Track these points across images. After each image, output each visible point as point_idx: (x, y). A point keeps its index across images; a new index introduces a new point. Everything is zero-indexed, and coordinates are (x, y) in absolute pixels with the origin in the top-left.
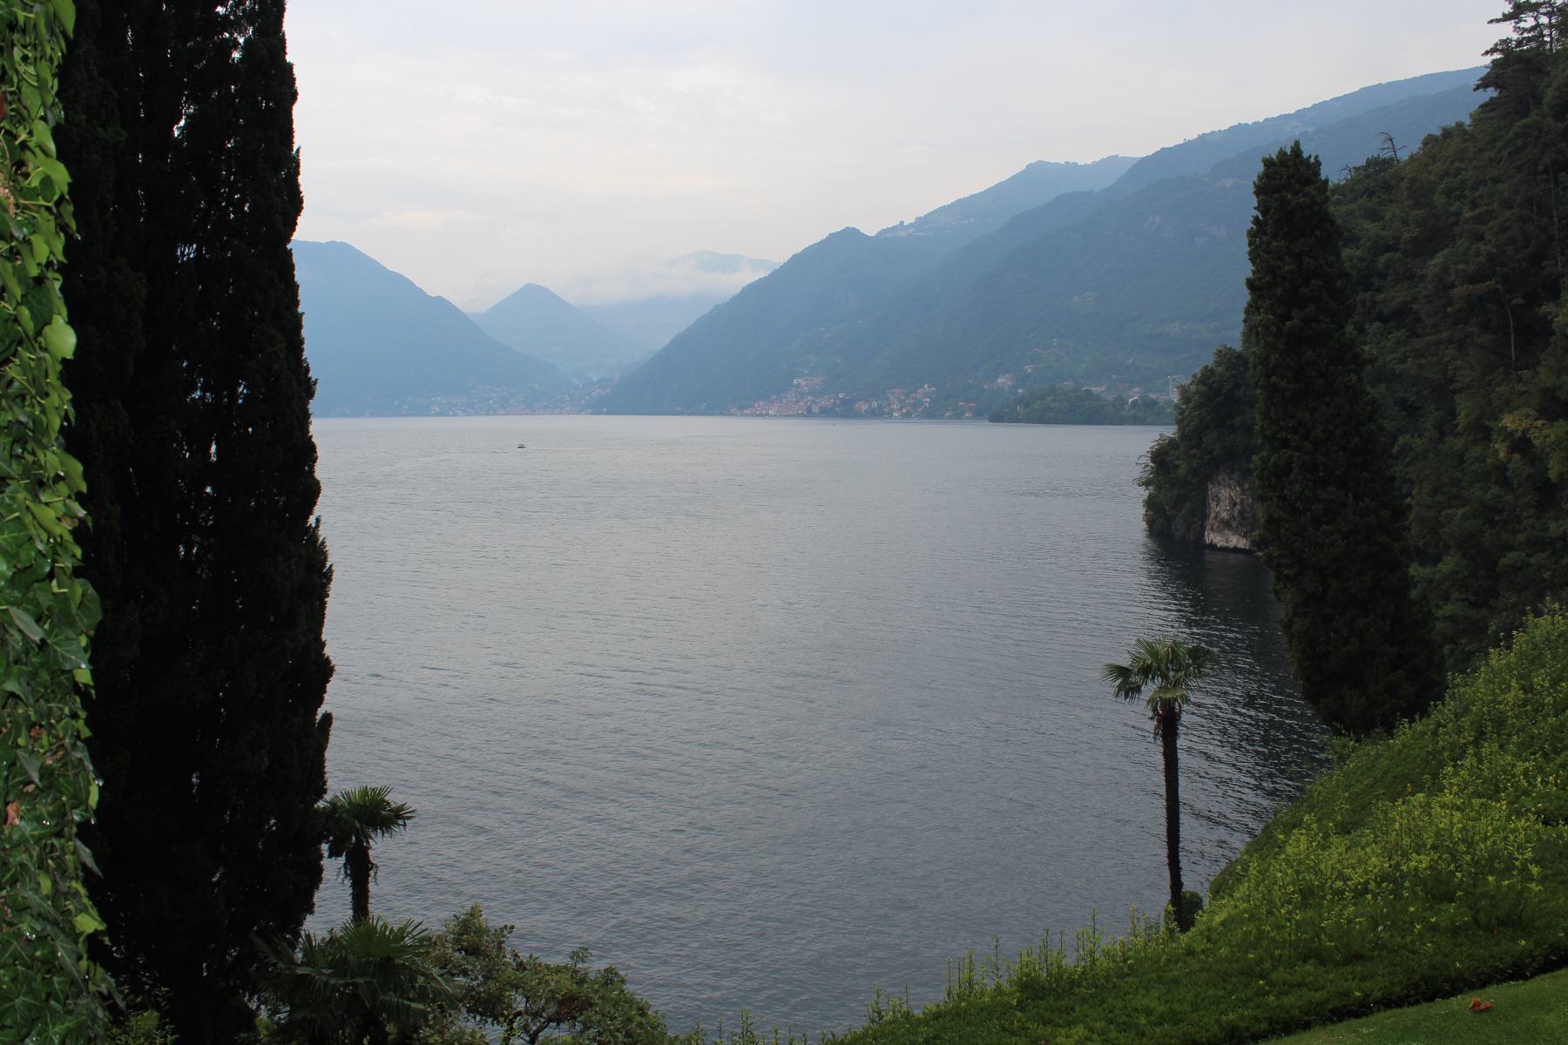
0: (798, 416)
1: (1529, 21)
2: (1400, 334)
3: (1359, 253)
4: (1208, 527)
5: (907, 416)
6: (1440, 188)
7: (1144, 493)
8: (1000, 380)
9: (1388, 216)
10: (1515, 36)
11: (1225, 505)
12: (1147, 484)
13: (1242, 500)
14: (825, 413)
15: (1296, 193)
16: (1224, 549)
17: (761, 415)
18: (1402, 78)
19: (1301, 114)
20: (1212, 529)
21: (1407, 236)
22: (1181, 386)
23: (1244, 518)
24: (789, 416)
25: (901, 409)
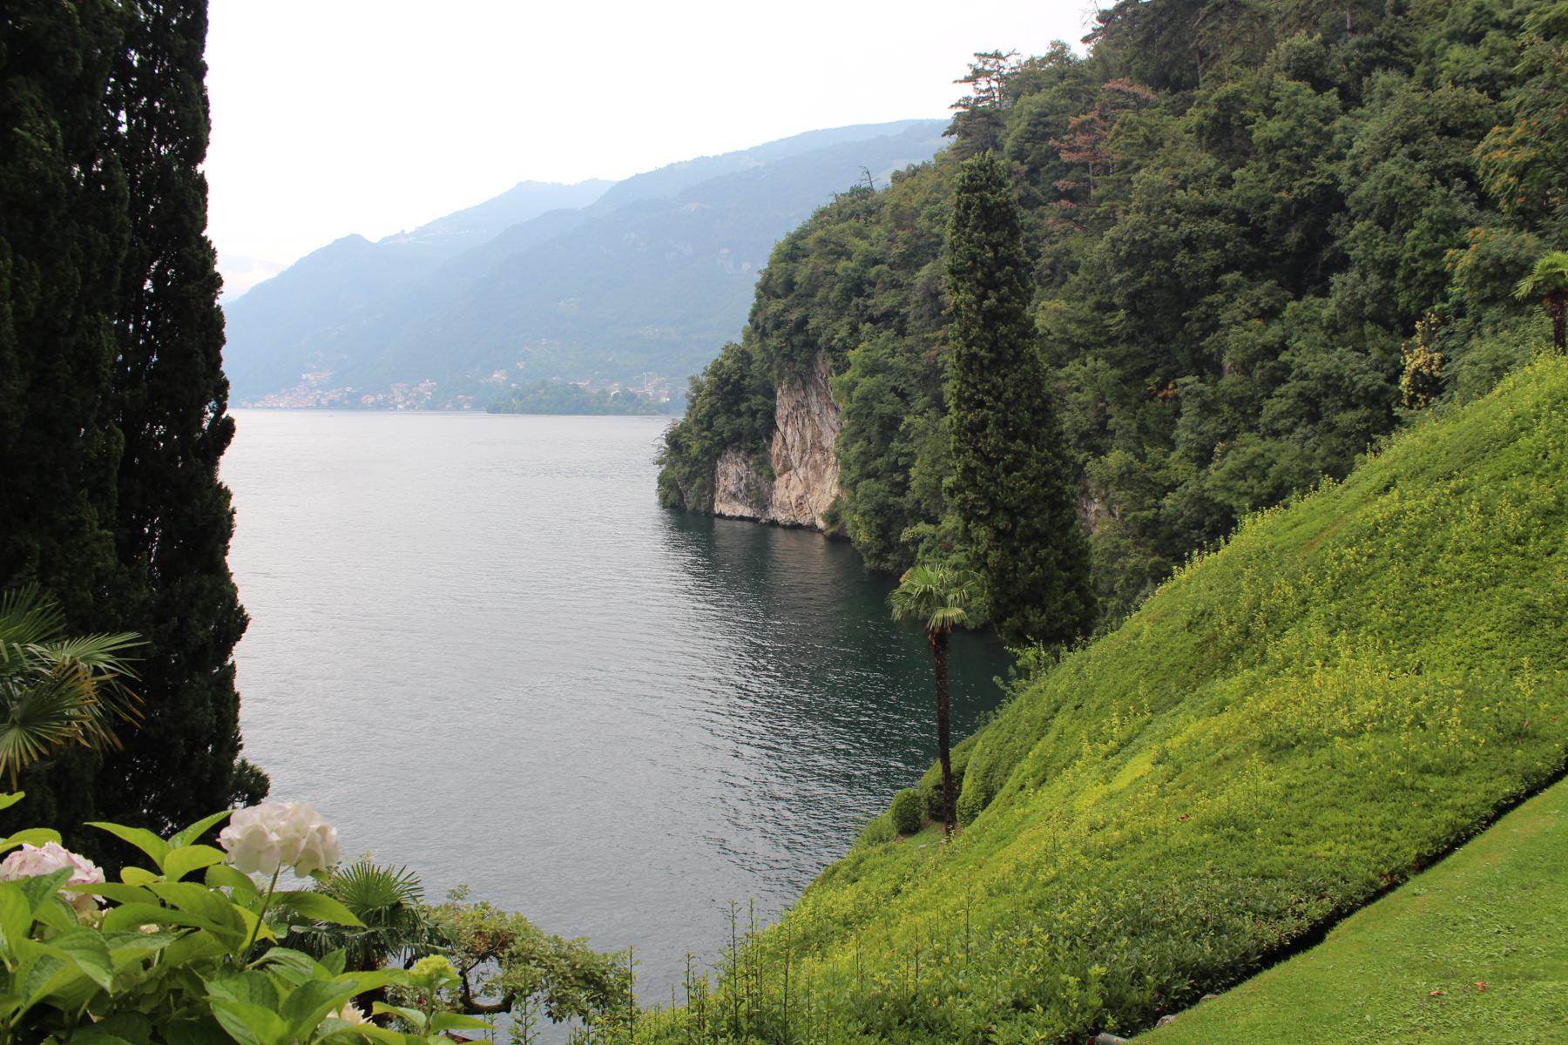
0: (307, 408)
1: (983, 84)
2: (891, 332)
3: (852, 265)
4: (717, 499)
5: (407, 408)
6: (924, 213)
7: (657, 471)
9: (874, 235)
10: (974, 95)
11: (733, 478)
12: (660, 463)
14: (333, 405)
15: (993, 193)
16: (731, 518)
17: (271, 408)
18: (834, 127)
19: (753, 152)
21: (895, 251)
22: (693, 378)
23: (750, 491)
24: (298, 408)
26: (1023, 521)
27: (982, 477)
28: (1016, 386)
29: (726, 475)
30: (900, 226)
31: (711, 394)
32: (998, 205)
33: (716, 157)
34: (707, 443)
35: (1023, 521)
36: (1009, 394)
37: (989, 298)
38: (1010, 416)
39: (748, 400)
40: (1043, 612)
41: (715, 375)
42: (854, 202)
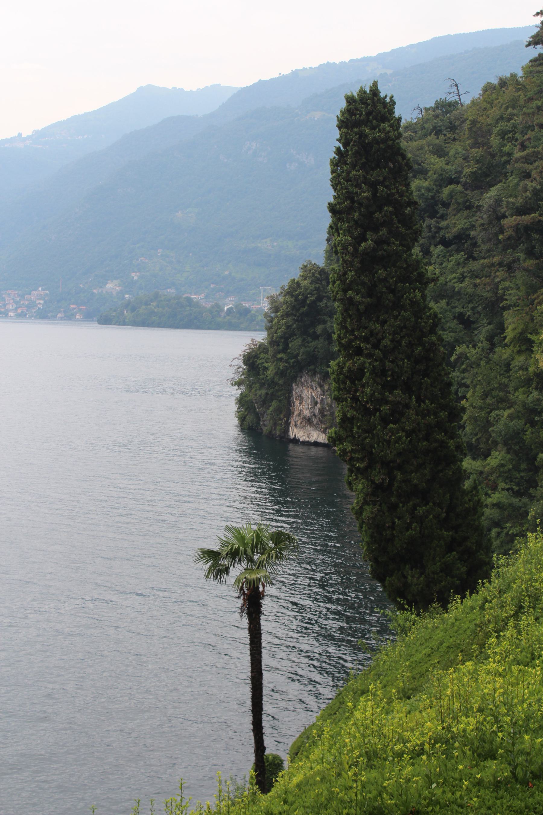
2: (460, 256)
3: (426, 184)
4: (292, 423)
5: (22, 316)
6: (496, 130)
8: (109, 286)
11: (307, 403)
12: (239, 384)
13: (322, 400)
15: (373, 128)
16: (306, 444)
20: (296, 425)
21: (467, 171)
22: (272, 297)
23: (324, 416)
25: (16, 309)
26: (399, 476)
27: (359, 428)
28: (395, 333)
29: (301, 399)
30: (476, 145)
31: (287, 315)
32: (376, 141)
33: (342, 64)
34: (282, 365)
35: (399, 476)
36: (386, 342)
37: (366, 240)
38: (388, 364)
39: (325, 322)
40: (421, 574)
41: (292, 296)
42: (437, 116)
